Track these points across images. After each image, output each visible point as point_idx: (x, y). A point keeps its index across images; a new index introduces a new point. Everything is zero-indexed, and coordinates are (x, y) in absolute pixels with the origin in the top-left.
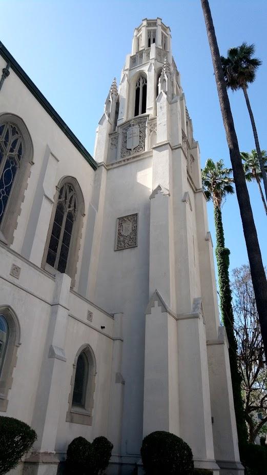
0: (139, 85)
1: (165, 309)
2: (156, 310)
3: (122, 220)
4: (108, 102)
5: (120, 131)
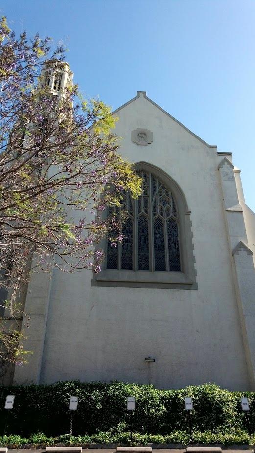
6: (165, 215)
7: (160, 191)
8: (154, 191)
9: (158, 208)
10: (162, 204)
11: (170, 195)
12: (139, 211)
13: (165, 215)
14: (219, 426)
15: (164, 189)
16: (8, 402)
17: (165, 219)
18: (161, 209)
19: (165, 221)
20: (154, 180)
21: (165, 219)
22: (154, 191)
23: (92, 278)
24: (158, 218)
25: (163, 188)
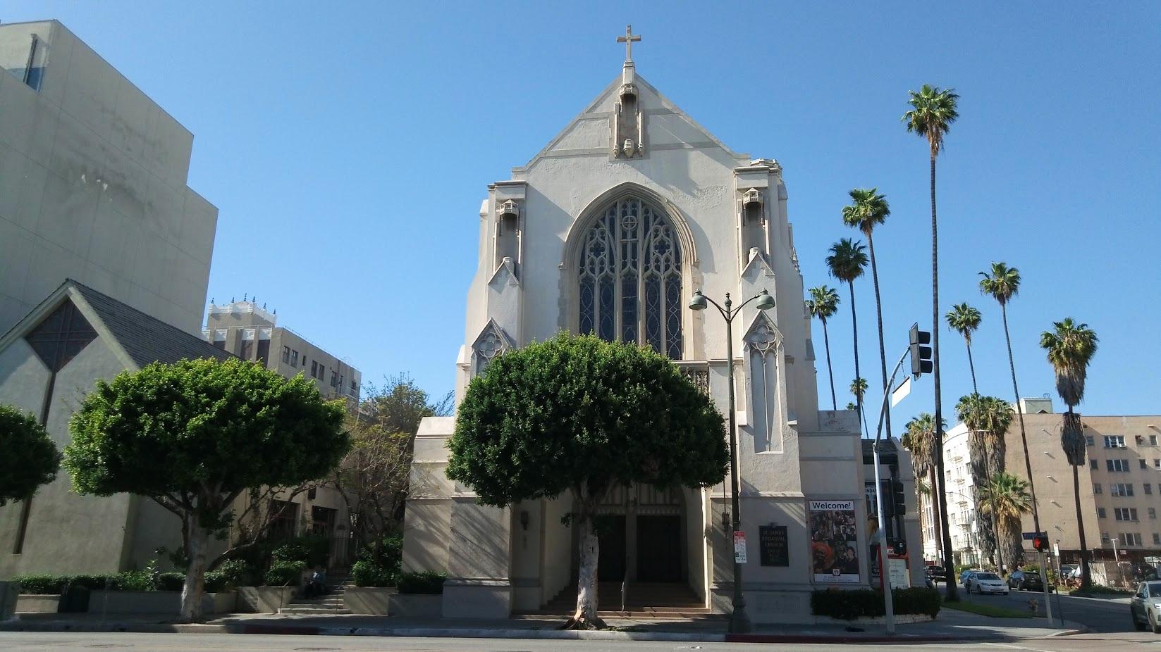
6: (597, 270)
7: (657, 231)
8: (647, 229)
9: (587, 261)
10: (592, 253)
11: (671, 235)
12: (624, 265)
13: (597, 270)
14: (183, 437)
15: (597, 228)
16: (418, 436)
17: (597, 278)
18: (592, 263)
19: (597, 281)
20: (647, 212)
21: (597, 278)
22: (647, 229)
23: (1085, 380)
24: (607, 275)
25: (662, 223)
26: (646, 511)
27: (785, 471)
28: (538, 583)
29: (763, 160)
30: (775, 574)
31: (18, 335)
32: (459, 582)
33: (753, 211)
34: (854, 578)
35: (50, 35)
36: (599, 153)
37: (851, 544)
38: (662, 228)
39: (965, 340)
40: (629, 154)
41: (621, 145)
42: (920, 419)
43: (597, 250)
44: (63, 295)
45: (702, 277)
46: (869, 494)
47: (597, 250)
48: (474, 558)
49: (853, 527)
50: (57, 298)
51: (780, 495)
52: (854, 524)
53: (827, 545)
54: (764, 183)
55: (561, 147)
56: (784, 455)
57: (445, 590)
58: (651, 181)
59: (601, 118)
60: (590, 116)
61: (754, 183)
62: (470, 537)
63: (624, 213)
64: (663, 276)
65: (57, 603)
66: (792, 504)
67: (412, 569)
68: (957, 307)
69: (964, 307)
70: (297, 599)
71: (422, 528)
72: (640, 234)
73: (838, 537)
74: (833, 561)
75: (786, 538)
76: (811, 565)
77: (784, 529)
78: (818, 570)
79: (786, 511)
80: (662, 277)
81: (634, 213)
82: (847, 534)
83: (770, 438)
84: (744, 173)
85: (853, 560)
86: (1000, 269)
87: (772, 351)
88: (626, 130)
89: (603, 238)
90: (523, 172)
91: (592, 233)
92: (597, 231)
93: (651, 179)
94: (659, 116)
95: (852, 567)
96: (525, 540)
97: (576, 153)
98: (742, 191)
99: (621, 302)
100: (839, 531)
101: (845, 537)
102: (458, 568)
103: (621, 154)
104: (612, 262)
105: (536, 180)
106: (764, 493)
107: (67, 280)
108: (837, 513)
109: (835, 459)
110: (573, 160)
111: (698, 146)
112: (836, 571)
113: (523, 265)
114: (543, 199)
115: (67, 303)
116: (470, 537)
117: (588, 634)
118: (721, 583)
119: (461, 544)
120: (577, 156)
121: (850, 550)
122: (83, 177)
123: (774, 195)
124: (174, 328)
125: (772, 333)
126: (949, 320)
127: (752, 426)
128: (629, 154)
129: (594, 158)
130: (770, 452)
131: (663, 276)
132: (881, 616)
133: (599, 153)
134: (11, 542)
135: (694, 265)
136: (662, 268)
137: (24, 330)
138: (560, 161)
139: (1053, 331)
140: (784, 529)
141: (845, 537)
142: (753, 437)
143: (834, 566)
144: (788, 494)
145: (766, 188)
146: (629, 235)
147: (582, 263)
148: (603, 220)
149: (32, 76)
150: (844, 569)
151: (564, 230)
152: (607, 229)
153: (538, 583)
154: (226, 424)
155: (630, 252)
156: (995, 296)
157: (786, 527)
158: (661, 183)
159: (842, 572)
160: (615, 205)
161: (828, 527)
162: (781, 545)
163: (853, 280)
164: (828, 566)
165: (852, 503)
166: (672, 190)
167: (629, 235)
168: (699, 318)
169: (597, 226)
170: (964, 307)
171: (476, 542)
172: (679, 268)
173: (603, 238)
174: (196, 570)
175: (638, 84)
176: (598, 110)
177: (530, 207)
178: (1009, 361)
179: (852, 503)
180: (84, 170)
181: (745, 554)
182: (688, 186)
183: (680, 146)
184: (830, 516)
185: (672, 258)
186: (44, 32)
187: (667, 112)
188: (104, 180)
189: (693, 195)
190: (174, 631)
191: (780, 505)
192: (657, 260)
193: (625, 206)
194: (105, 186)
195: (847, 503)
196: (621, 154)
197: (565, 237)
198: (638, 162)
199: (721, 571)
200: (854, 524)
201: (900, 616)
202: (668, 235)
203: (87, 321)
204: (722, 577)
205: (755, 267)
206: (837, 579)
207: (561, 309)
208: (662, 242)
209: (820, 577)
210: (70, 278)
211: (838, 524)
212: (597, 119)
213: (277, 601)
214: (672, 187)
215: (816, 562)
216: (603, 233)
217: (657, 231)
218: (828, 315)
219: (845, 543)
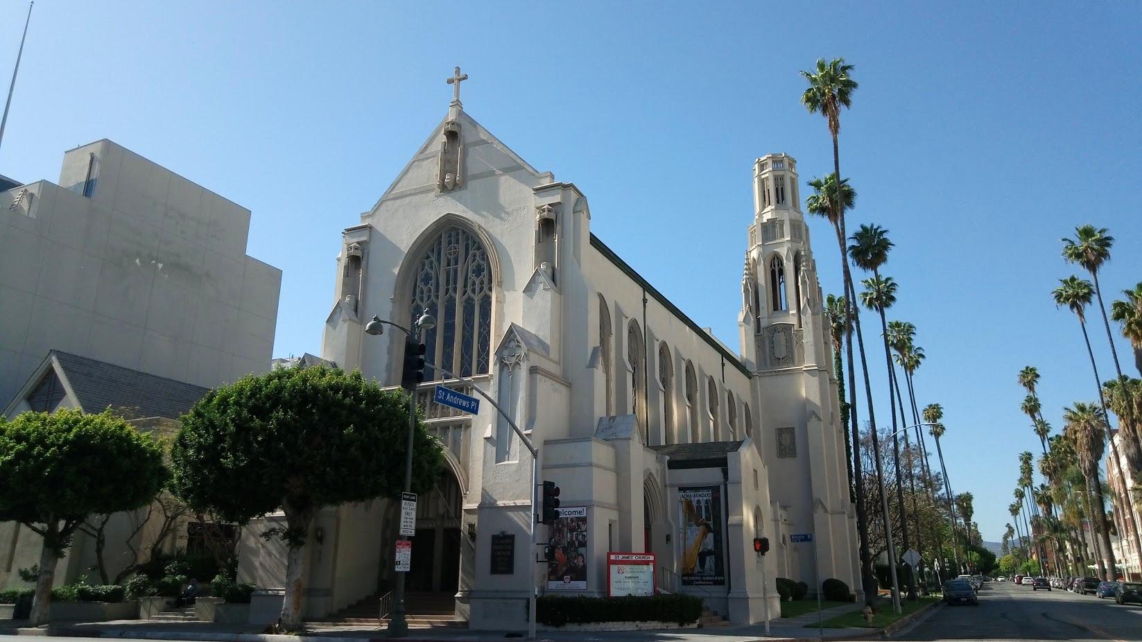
0: (774, 267)
1: (826, 511)
2: (820, 511)
3: (780, 432)
4: (746, 290)
5: (765, 334)
20: (467, 239)
26: (452, 524)
27: (518, 481)
28: (328, 593)
29: (770, 156)
30: (502, 582)
31: (21, 397)
32: (264, 592)
33: (547, 226)
34: (581, 585)
35: (101, 152)
36: (427, 190)
37: (582, 550)
38: (478, 253)
39: (1078, 316)
40: (450, 187)
41: (443, 179)
42: (1075, 410)
43: (427, 279)
44: (48, 364)
45: (504, 296)
46: (701, 499)
47: (427, 279)
48: (275, 571)
49: (585, 533)
50: (44, 366)
51: (511, 503)
52: (586, 531)
53: (561, 552)
54: (557, 198)
55: (399, 189)
56: (519, 464)
57: (253, 599)
58: (467, 209)
59: (431, 157)
60: (422, 156)
61: (546, 201)
62: (274, 552)
63: (450, 243)
64: (477, 299)
65: (12, 611)
66: (521, 513)
67: (243, 581)
68: (1065, 282)
69: (1073, 279)
70: (170, 608)
71: (253, 545)
72: (461, 260)
73: (571, 543)
74: (565, 569)
75: (513, 547)
76: (546, 573)
77: (512, 537)
78: (552, 577)
79: (516, 519)
80: (476, 299)
81: (457, 242)
82: (579, 541)
83: (509, 449)
84: (540, 191)
85: (582, 567)
86: (1087, 233)
87: (517, 363)
88: (448, 164)
89: (432, 268)
90: (369, 216)
91: (424, 265)
92: (427, 262)
93: (468, 208)
94: (477, 147)
95: (580, 574)
96: (321, 553)
97: (409, 192)
98: (540, 208)
99: (443, 325)
100: (572, 537)
101: (577, 543)
102: (264, 579)
103: (444, 188)
104: (437, 291)
105: (378, 223)
106: (500, 503)
107: (51, 350)
108: (572, 520)
109: (574, 466)
110: (407, 199)
111: (507, 170)
112: (567, 578)
113: (363, 302)
114: (384, 238)
115: (51, 372)
116: (274, 552)
117: (272, 638)
118: (466, 591)
119: (267, 558)
120: (410, 195)
121: (580, 557)
122: (138, 261)
123: (568, 210)
124: (157, 377)
125: (519, 346)
126: (1056, 297)
127: (495, 437)
128: (450, 187)
129: (423, 195)
130: (510, 462)
131: (477, 299)
132: (573, 623)
133: (427, 190)
134: (5, 565)
135: (498, 285)
136: (477, 290)
137: (25, 392)
138: (398, 201)
139: (1125, 299)
140: (512, 537)
141: (577, 543)
142: (494, 449)
143: (565, 573)
144: (519, 503)
145: (560, 203)
146: (452, 262)
147: (414, 294)
148: (433, 250)
149: (89, 186)
150: (574, 576)
151: (395, 266)
152: (434, 258)
153: (328, 593)
154: (19, 464)
155: (451, 279)
156: (1083, 264)
157: (514, 535)
158: (476, 212)
159: (572, 579)
160: (441, 236)
161: (563, 535)
162: (509, 553)
163: (877, 267)
164: (560, 573)
165: (585, 508)
166: (483, 216)
167: (452, 262)
168: (499, 336)
169: (428, 257)
170: (1073, 279)
171: (278, 556)
172: (490, 289)
173: (432, 268)
174: (43, 584)
175: (463, 122)
176: (428, 151)
177: (373, 248)
178: (1108, 338)
179: (585, 508)
180: (138, 255)
181: (409, 562)
182: (497, 210)
183: (492, 173)
184: (565, 523)
185: (486, 281)
186: (97, 150)
187: (484, 142)
188: (158, 261)
189: (502, 219)
190: (15, 633)
191: (511, 514)
192: (474, 284)
193: (450, 236)
194: (160, 266)
195: (581, 509)
196: (444, 188)
197: (396, 271)
198: (458, 193)
199: (467, 580)
200: (586, 531)
201: (615, 623)
202: (483, 259)
203: (60, 382)
204: (468, 586)
205: (534, 283)
206: (567, 586)
207: (390, 339)
208: (479, 266)
209: (554, 585)
210: (52, 349)
211: (572, 530)
212: (428, 158)
213: (153, 610)
214: (484, 213)
215: (550, 570)
216: (431, 263)
217: (475, 256)
218: (887, 306)
219: (576, 550)
